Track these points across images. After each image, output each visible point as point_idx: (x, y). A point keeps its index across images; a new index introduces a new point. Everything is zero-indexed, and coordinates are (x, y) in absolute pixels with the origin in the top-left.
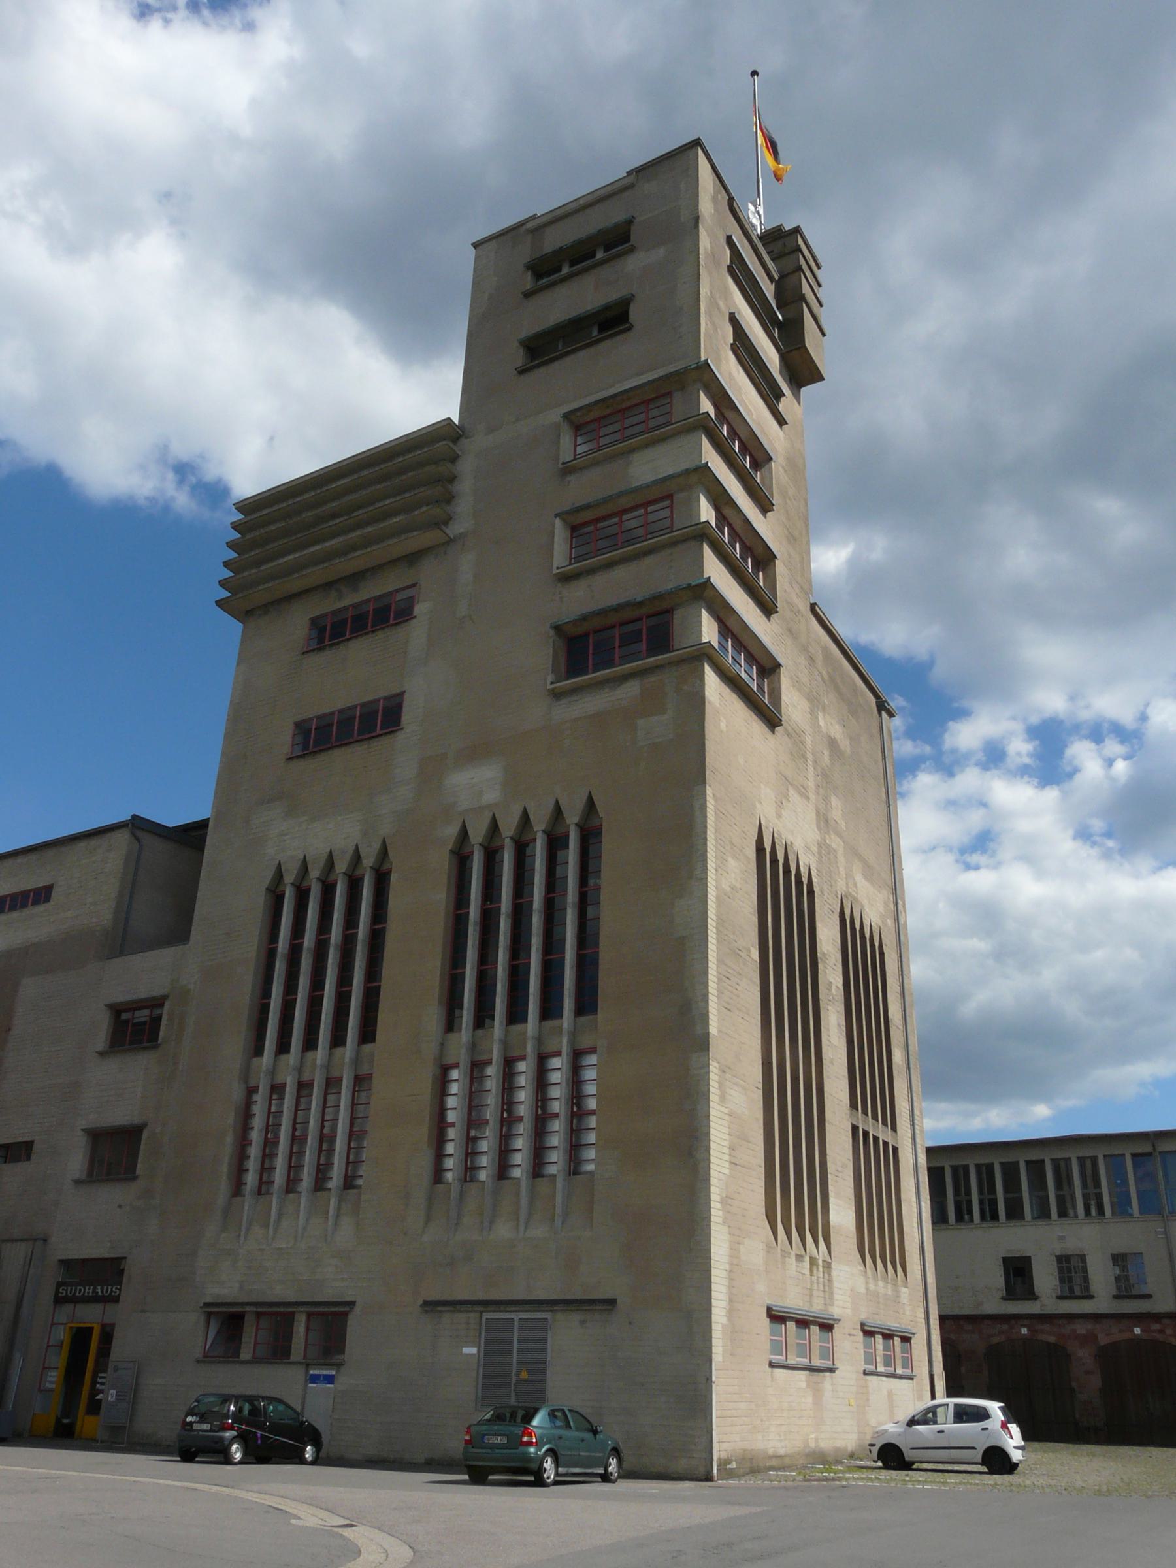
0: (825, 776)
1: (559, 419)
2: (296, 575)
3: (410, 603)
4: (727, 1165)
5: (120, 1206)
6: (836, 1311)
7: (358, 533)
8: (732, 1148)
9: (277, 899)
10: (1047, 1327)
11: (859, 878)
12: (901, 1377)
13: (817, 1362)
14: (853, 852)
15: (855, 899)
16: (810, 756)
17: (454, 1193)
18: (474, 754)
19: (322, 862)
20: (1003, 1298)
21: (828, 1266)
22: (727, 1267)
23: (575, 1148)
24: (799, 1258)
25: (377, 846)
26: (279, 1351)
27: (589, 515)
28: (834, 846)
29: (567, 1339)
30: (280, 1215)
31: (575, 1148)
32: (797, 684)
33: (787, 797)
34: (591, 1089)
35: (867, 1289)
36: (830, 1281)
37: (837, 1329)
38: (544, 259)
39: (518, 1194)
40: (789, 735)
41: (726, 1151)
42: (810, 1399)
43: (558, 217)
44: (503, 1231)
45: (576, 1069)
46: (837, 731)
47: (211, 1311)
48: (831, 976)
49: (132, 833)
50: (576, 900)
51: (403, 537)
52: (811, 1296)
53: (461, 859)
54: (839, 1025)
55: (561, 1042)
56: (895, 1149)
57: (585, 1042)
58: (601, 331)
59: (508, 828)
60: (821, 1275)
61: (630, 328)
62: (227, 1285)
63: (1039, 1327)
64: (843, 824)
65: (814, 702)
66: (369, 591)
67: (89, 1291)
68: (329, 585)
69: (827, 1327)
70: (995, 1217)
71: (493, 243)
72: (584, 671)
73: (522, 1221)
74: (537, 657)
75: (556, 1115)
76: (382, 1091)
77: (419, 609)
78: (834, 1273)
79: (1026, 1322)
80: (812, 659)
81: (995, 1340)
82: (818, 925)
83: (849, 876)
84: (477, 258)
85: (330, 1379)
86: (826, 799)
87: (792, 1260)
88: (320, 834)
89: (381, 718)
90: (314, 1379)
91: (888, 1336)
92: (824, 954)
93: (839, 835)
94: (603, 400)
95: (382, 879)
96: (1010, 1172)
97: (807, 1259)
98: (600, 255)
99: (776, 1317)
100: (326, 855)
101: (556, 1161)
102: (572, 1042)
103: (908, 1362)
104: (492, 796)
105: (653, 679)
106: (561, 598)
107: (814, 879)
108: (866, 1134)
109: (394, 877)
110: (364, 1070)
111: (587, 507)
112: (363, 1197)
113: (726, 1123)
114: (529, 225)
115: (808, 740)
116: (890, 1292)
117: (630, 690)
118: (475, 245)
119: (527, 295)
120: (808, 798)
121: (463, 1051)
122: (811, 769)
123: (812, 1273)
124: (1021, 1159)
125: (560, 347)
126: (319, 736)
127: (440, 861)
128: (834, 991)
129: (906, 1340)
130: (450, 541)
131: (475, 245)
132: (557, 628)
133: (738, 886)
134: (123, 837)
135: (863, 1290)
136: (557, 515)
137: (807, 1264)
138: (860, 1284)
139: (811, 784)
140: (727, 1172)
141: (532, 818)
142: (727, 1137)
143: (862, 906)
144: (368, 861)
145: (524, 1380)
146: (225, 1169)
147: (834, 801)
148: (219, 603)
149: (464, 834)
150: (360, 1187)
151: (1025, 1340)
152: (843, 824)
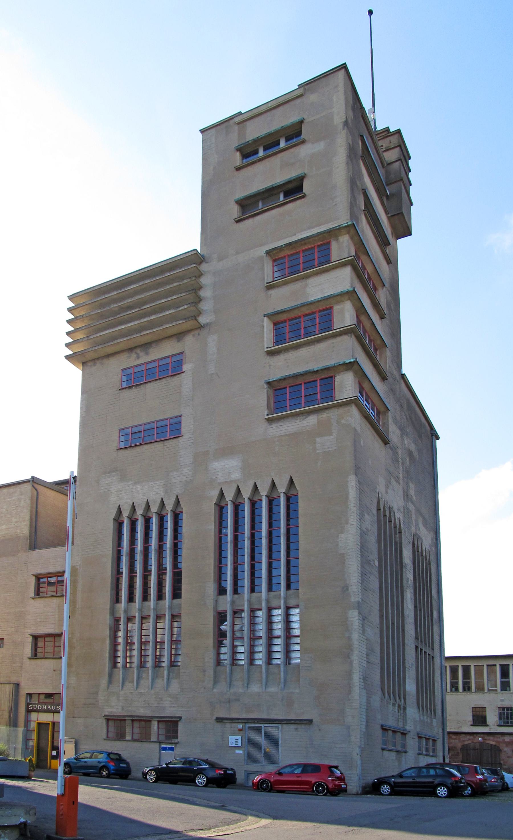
0: (407, 472)
1: (263, 254)
2: (111, 343)
3: (180, 363)
4: (365, 662)
5: (54, 671)
6: (408, 728)
7: (147, 319)
8: (367, 655)
9: (120, 525)
10: (491, 738)
11: (421, 526)
12: (432, 756)
13: (400, 749)
14: (419, 512)
15: (419, 536)
16: (400, 460)
17: (228, 670)
18: (225, 452)
19: (143, 507)
20: (472, 725)
21: (405, 709)
22: (366, 707)
23: (288, 651)
24: (394, 705)
25: (173, 499)
26: (145, 738)
27: (284, 317)
28: (410, 508)
29: (287, 735)
30: (139, 678)
31: (288, 651)
32: (395, 420)
33: (390, 482)
34: (295, 625)
35: (420, 719)
36: (406, 715)
37: (407, 736)
38: (248, 145)
39: (261, 672)
40: (391, 449)
41: (365, 656)
42: (397, 764)
43: (256, 114)
44: (255, 688)
45: (287, 615)
46: (413, 447)
47: (109, 719)
48: (409, 575)
49: (33, 486)
50: (285, 532)
51: (174, 323)
52: (398, 721)
53: (221, 509)
54: (411, 599)
55: (280, 602)
56: (433, 657)
57: (292, 602)
58: (285, 196)
59: (246, 493)
60: (402, 712)
61: (303, 197)
62: (115, 708)
63: (487, 738)
64: (414, 497)
65: (402, 429)
66: (157, 353)
67: (45, 707)
68: (131, 350)
69: (404, 734)
70: (457, 689)
71: (213, 131)
72: (283, 408)
73: (264, 684)
74: (260, 400)
75: (261, 638)
76: (186, 621)
77: (186, 367)
78: (407, 712)
79: (481, 735)
80: (401, 406)
81: (466, 743)
82: (404, 549)
83: (417, 525)
84: (204, 141)
85: (172, 749)
86: (407, 484)
87: (391, 706)
88: (144, 492)
89: (169, 430)
90: (164, 749)
91: (427, 739)
92: (406, 564)
93: (413, 503)
94: (290, 244)
95: (177, 517)
96: (466, 670)
97: (397, 705)
98: (261, 153)
99: (384, 729)
100: (145, 503)
101: (278, 658)
102: (285, 602)
103: (434, 751)
104: (236, 475)
105: (324, 416)
106: (270, 365)
107: (402, 526)
108: (421, 649)
109: (184, 516)
110: (176, 612)
111: (283, 312)
112: (181, 671)
113: (365, 643)
114: (237, 120)
115: (400, 452)
116: (429, 721)
117: (312, 420)
118: (202, 131)
119: (238, 169)
120: (399, 483)
121: (229, 605)
122: (401, 468)
123: (398, 712)
124: (460, 664)
125: (260, 207)
126: (136, 438)
127: (210, 509)
128: (409, 582)
129: (434, 741)
130: (201, 327)
131: (202, 131)
132: (269, 383)
133: (369, 528)
134: (28, 487)
135: (418, 719)
136: (265, 316)
137: (397, 708)
138: (417, 716)
139: (401, 476)
140: (365, 665)
141: (259, 488)
142: (365, 650)
143: (422, 540)
144: (169, 506)
145: (268, 752)
146: (107, 655)
147: (411, 485)
148: (67, 357)
149: (222, 494)
150: (179, 666)
151: (481, 743)
152: (414, 497)
